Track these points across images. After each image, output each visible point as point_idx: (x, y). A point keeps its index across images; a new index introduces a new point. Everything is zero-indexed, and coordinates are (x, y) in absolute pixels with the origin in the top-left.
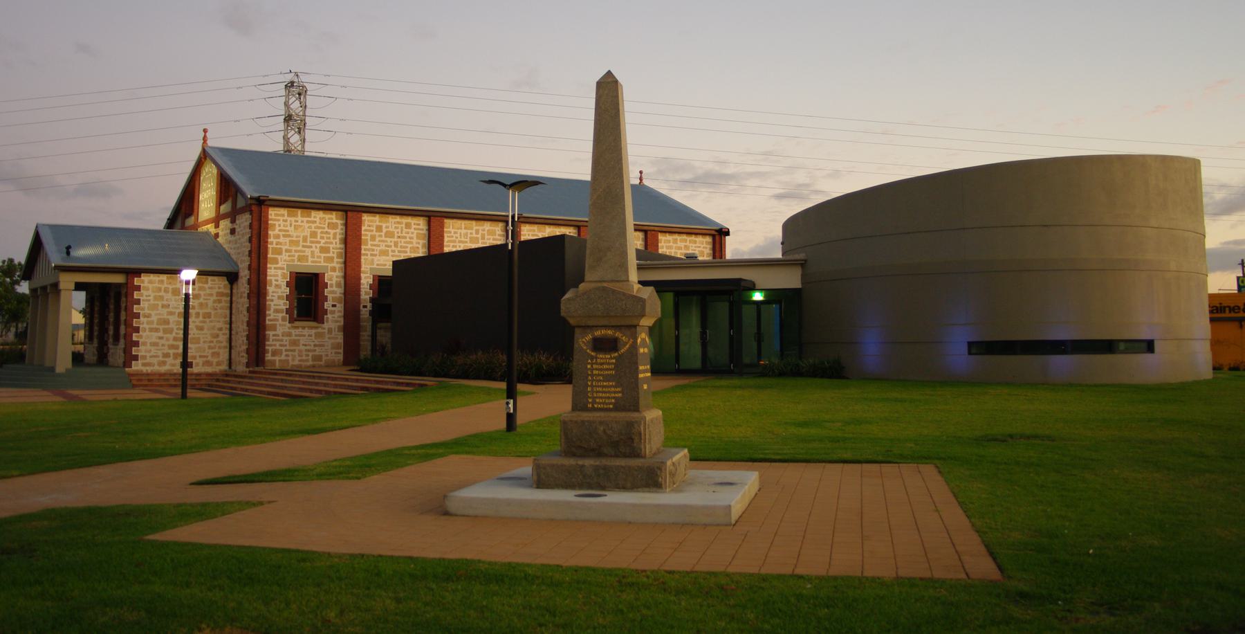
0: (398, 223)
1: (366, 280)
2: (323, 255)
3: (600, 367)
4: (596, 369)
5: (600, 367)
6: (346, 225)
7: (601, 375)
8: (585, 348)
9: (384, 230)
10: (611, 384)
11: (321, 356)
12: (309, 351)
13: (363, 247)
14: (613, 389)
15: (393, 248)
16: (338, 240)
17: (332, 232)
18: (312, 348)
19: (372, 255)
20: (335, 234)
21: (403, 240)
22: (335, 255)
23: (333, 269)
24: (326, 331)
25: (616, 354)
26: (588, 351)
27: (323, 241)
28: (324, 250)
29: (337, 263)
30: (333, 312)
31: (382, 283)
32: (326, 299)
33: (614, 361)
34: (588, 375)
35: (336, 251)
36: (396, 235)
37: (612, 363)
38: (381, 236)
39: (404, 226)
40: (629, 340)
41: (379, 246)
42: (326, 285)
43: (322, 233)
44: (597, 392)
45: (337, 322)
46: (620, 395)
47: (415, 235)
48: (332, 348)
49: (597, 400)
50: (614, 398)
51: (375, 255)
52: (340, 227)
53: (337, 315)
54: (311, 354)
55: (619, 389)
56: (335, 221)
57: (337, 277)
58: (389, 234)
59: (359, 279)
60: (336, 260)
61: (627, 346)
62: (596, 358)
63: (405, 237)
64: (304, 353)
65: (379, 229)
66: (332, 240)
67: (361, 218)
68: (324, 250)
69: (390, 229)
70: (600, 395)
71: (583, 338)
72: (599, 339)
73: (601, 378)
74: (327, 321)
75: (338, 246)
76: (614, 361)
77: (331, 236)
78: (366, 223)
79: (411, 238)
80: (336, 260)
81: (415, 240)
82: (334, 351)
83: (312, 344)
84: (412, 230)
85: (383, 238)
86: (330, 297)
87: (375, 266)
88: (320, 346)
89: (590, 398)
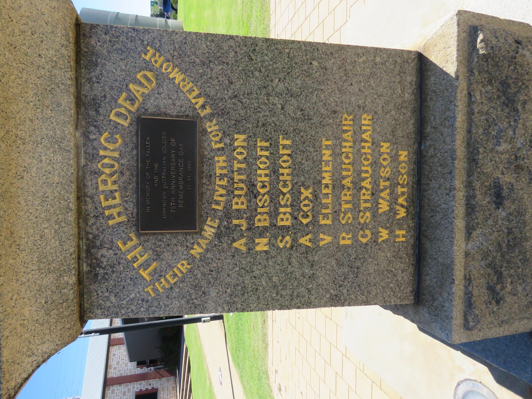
0: (112, 360)
1: (139, 371)
2: (127, 394)
3: (263, 201)
4: (274, 214)
5: (263, 201)
6: (112, 385)
7: (296, 194)
8: (183, 267)
9: (116, 366)
10: (327, 154)
11: (172, 387)
12: (170, 393)
13: (123, 375)
14: (347, 147)
15: (124, 361)
16: (120, 388)
17: (116, 391)
18: (169, 392)
19: (127, 370)
20: (117, 390)
21: (121, 356)
22: (127, 388)
23: (133, 388)
24: (161, 386)
25: (211, 127)
26: (197, 251)
27: (120, 395)
28: (124, 394)
29: (130, 386)
30: (153, 384)
31: (140, 364)
32: (147, 389)
33: (240, 139)
34: (295, 245)
35: (125, 388)
36: (118, 360)
37: (251, 147)
38: (119, 367)
39: (114, 357)
40: (148, 66)
41: (123, 368)
42: (141, 390)
43: (116, 397)
44: (356, 209)
45: (157, 382)
46: (366, 120)
47: (119, 351)
48: (169, 382)
49: (384, 207)
50: (375, 144)
51: (127, 368)
52: (114, 388)
53: (154, 383)
54: (171, 392)
55: (347, 121)
56: (111, 391)
57: (137, 385)
58: (118, 363)
59: (138, 375)
60: (129, 387)
61: (177, 76)
62: (228, 214)
63: (119, 356)
64: (171, 395)
65: (115, 368)
66: (120, 391)
67: (110, 378)
68: (124, 394)
69: (116, 364)
70: (365, 195)
71: (136, 280)
72: (141, 204)
73: (306, 193)
74: (157, 386)
75: (123, 387)
76: (240, 139)
77: (118, 391)
78: (112, 375)
79: (120, 353)
80: (129, 387)
81: (121, 351)
82: (170, 381)
83: (167, 392)
84: (116, 353)
85: (120, 366)
86: (146, 387)
87: (132, 368)
88: (168, 388)
89: (376, 234)
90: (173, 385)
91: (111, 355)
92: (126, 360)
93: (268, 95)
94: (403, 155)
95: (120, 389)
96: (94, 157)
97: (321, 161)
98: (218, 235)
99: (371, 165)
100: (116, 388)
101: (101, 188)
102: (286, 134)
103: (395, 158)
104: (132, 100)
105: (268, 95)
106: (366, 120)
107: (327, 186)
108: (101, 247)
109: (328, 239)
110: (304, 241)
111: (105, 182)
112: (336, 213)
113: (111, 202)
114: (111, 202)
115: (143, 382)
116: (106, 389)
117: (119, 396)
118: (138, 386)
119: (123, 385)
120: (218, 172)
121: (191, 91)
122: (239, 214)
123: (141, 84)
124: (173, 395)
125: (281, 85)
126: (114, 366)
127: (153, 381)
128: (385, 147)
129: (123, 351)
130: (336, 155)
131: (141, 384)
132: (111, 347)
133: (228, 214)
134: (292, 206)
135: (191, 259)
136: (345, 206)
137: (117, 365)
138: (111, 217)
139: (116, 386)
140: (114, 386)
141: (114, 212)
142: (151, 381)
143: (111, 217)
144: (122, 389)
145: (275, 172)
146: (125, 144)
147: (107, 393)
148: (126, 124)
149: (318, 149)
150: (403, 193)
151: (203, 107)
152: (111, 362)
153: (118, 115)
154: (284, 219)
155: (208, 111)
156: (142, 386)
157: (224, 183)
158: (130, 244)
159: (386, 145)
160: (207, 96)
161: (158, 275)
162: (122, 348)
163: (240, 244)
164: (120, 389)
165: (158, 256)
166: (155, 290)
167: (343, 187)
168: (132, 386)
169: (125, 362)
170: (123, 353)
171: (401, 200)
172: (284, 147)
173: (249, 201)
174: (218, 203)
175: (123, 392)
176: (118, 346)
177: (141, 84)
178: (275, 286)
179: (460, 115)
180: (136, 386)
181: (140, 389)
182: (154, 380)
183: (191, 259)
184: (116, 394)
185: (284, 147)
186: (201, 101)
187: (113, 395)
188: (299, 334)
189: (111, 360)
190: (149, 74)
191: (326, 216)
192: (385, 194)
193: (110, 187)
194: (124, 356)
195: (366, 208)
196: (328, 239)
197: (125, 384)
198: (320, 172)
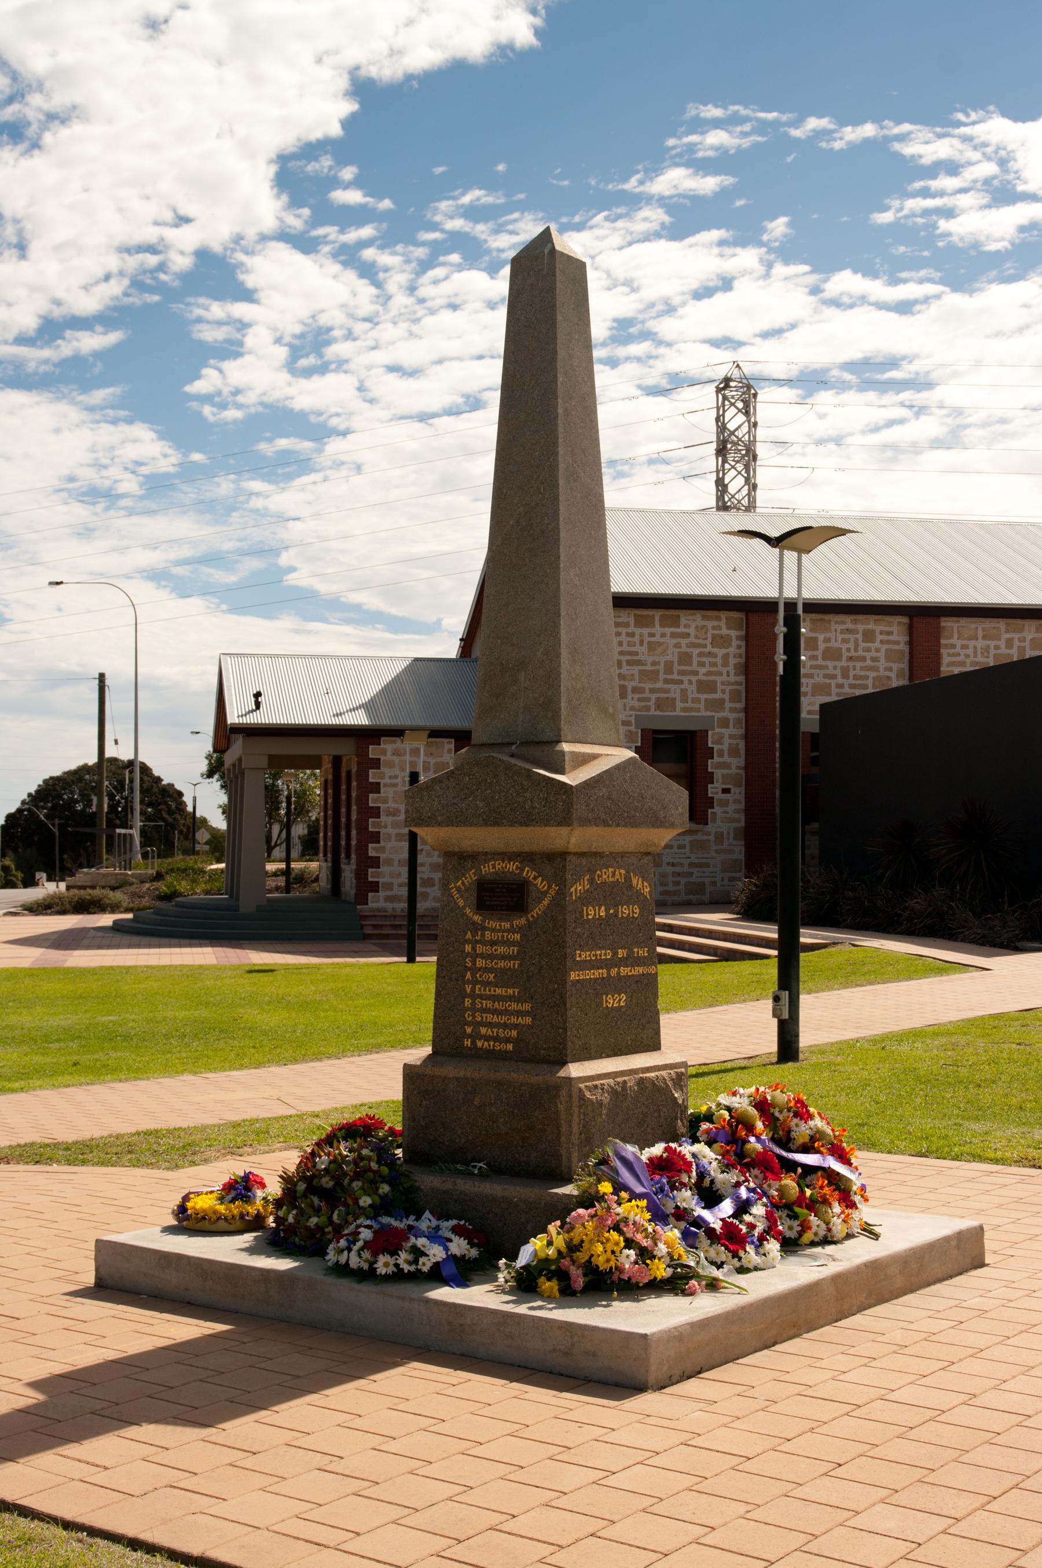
0: (849, 631)
2: (703, 697)
4: (483, 956)
6: (747, 638)
8: (461, 903)
9: (822, 646)
10: (510, 991)
14: (514, 1006)
16: (731, 669)
17: (721, 652)
18: (686, 869)
20: (726, 657)
21: (859, 664)
22: (726, 697)
23: (724, 723)
24: (712, 838)
25: (523, 921)
26: (468, 911)
28: (706, 687)
29: (731, 710)
30: (724, 803)
32: (710, 778)
34: (467, 969)
35: (728, 688)
37: (514, 943)
39: (860, 637)
40: (550, 887)
43: (701, 655)
45: (732, 820)
46: (528, 1020)
47: (882, 655)
49: (483, 1031)
50: (516, 1026)
53: (731, 807)
54: (683, 881)
55: (527, 1007)
57: (731, 737)
58: (833, 654)
60: (728, 705)
61: (546, 902)
62: (484, 929)
63: (864, 659)
66: (720, 668)
69: (833, 644)
71: (457, 879)
74: (714, 821)
75: (733, 678)
76: (517, 936)
77: (719, 660)
79: (874, 659)
80: (728, 705)
81: (882, 664)
84: (877, 644)
85: (820, 662)
86: (718, 774)
89: (468, 1024)
90: (709, 889)
91: (870, 623)
92: (840, 686)
93: (539, 955)
94: (510, 1047)
95: (724, 670)
96: (510, 860)
97: (507, 987)
98: (474, 923)
99: (505, 1023)
100: (735, 651)
101: (497, 862)
102: (520, 965)
103: (508, 1040)
104: (535, 878)
105: (539, 955)
106: (528, 1020)
107: (495, 991)
108: (472, 862)
109: (468, 990)
110: (468, 976)
111: (499, 864)
112: (481, 997)
113: (491, 867)
114: (491, 867)
115: (741, 761)
116: (735, 615)
117: (701, 664)
118: (727, 741)
119: (741, 678)
120: (503, 924)
121: (539, 909)
122: (483, 935)
123: (542, 883)
124: (671, 888)
125: (544, 963)
126: (821, 637)
127: (736, 801)
128: (514, 1033)
129: (882, 673)
130: (511, 998)
131: (734, 752)
132: (905, 620)
133: (484, 929)
134: (486, 967)
135: (464, 907)
136: (484, 1002)
137: (827, 650)
138: (484, 867)
139: (743, 651)
140: (743, 643)
141: (487, 869)
142: (738, 793)
143: (484, 867)
144: (724, 678)
145: (503, 957)
146: (515, 875)
147: (718, 619)
148: (524, 875)
149: (513, 986)
150: (490, 1046)
151: (532, 916)
152: (839, 624)
153: (528, 871)
154: (480, 963)
155: (531, 919)
156: (726, 758)
157: (498, 927)
158: (473, 876)
159: (515, 1034)
160: (537, 919)
161: (459, 890)
162: (895, 666)
163: (469, 935)
164: (724, 670)
165: (467, 890)
166: (452, 888)
167: (494, 1002)
168: (731, 716)
169: (833, 682)
170: (872, 674)
171: (486, 1043)
172: (514, 964)
173: (489, 942)
174: (488, 923)
175: (715, 682)
176: (906, 649)
177: (542, 883)
178: (448, 956)
179: (514, 1075)
180: (726, 732)
181: (716, 747)
182: (742, 806)
183: (464, 907)
184: (710, 654)
185: (514, 964)
186: (535, 915)
187: (708, 642)
188: (825, 1474)
189: (849, 625)
190: (546, 887)
191: (480, 990)
192: (490, 1032)
193: (497, 867)
194: (861, 678)
195: (482, 1017)
196: (468, 990)
197: (742, 688)
198: (502, 987)
